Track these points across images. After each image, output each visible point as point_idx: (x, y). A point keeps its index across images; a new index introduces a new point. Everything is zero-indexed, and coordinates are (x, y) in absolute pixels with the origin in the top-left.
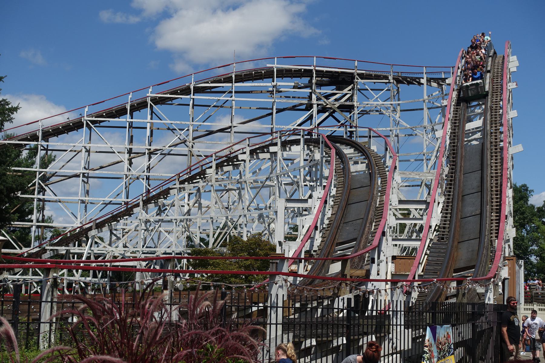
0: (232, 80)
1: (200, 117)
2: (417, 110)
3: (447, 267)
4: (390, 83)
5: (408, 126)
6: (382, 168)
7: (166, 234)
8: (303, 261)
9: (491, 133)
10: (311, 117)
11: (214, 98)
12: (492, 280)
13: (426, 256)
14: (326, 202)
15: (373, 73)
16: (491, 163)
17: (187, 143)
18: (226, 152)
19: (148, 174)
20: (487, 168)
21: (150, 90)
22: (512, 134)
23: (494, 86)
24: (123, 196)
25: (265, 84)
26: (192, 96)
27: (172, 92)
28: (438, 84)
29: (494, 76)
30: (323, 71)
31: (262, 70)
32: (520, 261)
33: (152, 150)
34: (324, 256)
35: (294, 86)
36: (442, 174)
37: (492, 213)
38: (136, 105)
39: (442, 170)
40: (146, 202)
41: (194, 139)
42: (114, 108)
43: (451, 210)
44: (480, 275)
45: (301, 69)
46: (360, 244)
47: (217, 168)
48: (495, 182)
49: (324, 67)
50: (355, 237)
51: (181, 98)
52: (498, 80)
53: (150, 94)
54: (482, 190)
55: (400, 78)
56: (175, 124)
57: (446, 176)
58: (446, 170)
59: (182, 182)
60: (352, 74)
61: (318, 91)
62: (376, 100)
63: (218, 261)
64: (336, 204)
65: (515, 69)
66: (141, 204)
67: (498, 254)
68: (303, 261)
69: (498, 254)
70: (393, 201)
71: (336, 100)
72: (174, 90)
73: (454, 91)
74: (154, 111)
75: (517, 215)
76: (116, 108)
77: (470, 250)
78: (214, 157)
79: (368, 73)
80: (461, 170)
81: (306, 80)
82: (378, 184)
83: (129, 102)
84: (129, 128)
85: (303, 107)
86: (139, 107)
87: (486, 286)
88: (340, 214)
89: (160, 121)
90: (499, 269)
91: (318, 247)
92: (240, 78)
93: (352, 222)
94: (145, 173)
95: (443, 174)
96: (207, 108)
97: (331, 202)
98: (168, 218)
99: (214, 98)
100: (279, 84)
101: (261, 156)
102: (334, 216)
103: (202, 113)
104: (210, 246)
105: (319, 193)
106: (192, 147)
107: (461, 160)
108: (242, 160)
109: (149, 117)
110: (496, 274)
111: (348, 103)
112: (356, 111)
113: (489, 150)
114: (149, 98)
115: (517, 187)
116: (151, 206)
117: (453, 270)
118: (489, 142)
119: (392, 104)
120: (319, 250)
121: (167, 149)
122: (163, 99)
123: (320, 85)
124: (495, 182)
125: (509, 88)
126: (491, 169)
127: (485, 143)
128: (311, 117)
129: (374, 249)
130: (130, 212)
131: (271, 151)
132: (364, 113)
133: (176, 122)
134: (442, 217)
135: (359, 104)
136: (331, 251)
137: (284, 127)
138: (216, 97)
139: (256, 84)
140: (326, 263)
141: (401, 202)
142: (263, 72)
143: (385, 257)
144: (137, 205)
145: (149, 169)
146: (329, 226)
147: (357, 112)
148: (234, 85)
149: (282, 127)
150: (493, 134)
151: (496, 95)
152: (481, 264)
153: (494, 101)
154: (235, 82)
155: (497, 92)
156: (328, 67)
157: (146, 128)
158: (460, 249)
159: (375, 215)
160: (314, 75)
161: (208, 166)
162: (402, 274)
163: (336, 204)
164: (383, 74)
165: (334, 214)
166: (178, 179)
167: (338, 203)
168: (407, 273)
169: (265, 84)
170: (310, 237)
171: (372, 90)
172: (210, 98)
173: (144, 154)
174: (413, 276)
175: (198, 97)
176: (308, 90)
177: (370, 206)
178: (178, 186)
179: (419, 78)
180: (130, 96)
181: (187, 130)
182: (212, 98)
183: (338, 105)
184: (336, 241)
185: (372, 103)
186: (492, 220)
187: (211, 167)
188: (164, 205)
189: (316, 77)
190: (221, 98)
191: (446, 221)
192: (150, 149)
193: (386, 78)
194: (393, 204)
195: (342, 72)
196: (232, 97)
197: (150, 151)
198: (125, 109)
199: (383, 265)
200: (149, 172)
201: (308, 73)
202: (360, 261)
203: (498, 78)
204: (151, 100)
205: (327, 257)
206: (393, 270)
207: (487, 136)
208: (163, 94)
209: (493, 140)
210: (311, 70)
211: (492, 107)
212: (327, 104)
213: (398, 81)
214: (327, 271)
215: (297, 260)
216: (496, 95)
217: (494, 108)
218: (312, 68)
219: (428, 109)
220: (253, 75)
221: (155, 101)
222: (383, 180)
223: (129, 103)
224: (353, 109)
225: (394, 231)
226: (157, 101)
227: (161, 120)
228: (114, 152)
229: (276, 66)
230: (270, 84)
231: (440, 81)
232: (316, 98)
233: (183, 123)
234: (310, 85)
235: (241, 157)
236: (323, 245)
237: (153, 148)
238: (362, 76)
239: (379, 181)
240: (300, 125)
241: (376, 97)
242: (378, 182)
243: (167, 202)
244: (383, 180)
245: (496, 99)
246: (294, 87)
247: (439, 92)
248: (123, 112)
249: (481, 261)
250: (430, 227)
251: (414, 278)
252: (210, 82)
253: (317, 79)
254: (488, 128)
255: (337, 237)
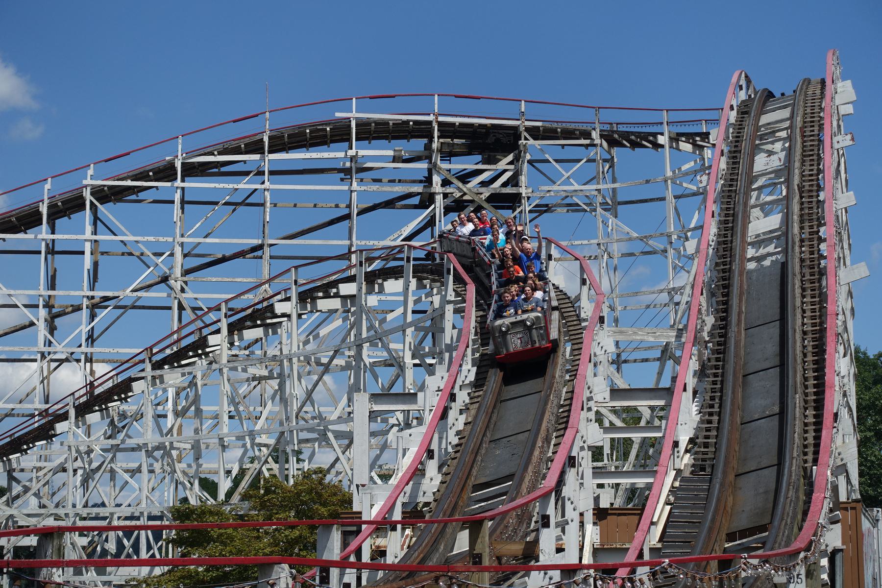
0: (263, 148)
1: (197, 226)
2: (652, 200)
3: (710, 529)
4: (595, 145)
5: (635, 235)
6: (575, 323)
7: (127, 476)
8: (399, 526)
9: (802, 241)
10: (431, 222)
11: (226, 186)
12: (802, 555)
13: (668, 508)
14: (453, 397)
15: (559, 127)
16: (803, 303)
17: (172, 282)
18: (250, 298)
19: (89, 350)
20: (795, 315)
21: (90, 172)
22: (850, 245)
23: (805, 142)
24: (37, 400)
25: (332, 155)
26: (178, 183)
27: (136, 175)
28: (694, 144)
29: (805, 122)
30: (453, 124)
31: (326, 124)
32: (875, 509)
33: (97, 300)
34: (444, 515)
35: (394, 157)
36: (702, 330)
37: (806, 409)
38: (60, 204)
39: (700, 321)
40: (83, 410)
41: (186, 272)
42: (14, 213)
43: (720, 407)
44: (780, 544)
45: (408, 122)
46: (521, 485)
47: (231, 332)
48: (811, 343)
49: (456, 116)
50: (512, 471)
51: (157, 187)
52: (813, 131)
53: (90, 179)
54: (783, 365)
55: (616, 136)
56: (143, 243)
57: (711, 334)
58: (710, 320)
59: (158, 366)
60: (515, 128)
61: (445, 166)
62: (567, 182)
63: (230, 531)
64: (476, 400)
65: (849, 109)
66: (72, 413)
67: (818, 497)
68: (399, 526)
69: (818, 497)
70: (596, 390)
71: (483, 184)
72: (142, 170)
73: (722, 155)
74: (99, 215)
75: (870, 415)
76: (17, 211)
77: (761, 490)
78: (224, 310)
79: (548, 125)
80: (739, 321)
81: (418, 144)
82: (564, 355)
83: (46, 197)
84: (47, 253)
85: (416, 200)
86: (68, 209)
87: (788, 570)
88: (481, 424)
89: (113, 238)
90: (818, 530)
91: (434, 493)
92: (279, 144)
93: (508, 439)
94: (84, 349)
95: (703, 330)
96: (212, 206)
97: (463, 397)
98: (131, 442)
99: (226, 186)
100: (361, 153)
101: (324, 304)
102: (469, 427)
103: (201, 217)
104: (222, 496)
105: (437, 381)
106: (183, 290)
107: (740, 300)
108: (284, 315)
109: (89, 228)
110: (811, 542)
111: (509, 190)
112: (527, 206)
113: (799, 277)
114: (89, 189)
115: (868, 357)
116: (94, 418)
117: (724, 536)
118: (797, 260)
119: (599, 190)
120: (435, 500)
121: (127, 294)
122: (117, 189)
123: (448, 154)
124: (811, 343)
125: (836, 146)
126: (803, 317)
127: (790, 263)
128: (431, 222)
129: (546, 496)
130: (49, 430)
131: (342, 294)
132: (542, 209)
133: (146, 238)
134: (702, 421)
135: (530, 190)
136: (460, 503)
137: (376, 243)
138: (228, 183)
139: (314, 155)
140: (449, 530)
141: (616, 393)
142: (328, 129)
143: (577, 513)
144: (64, 417)
145: (91, 338)
146: (459, 448)
147: (528, 209)
148: (267, 159)
149: (371, 243)
150: (807, 243)
151: (811, 160)
152: (782, 519)
153: (807, 173)
154: (270, 152)
155: (812, 155)
156: (464, 116)
157: (83, 253)
158: (740, 489)
159: (556, 422)
160: (436, 134)
161: (214, 328)
162: (616, 549)
163: (476, 400)
164: (581, 128)
165: (470, 423)
166: (150, 359)
167: (479, 399)
168: (627, 546)
169: (332, 155)
170: (417, 472)
171: (557, 161)
172: (217, 185)
173: (78, 308)
174: (637, 552)
175: (194, 184)
176: (423, 165)
177: (546, 403)
178: (149, 371)
179: (655, 135)
180: (48, 186)
181: (169, 256)
182: (221, 186)
183: (487, 195)
184: (472, 481)
185: (554, 191)
186: (806, 425)
187: (218, 331)
188: (123, 416)
189: (439, 137)
190: (241, 186)
191: (710, 431)
192: (93, 298)
193: (587, 135)
194: (598, 397)
195: (493, 125)
196: (263, 183)
197: (93, 301)
198: (39, 214)
199: (573, 528)
200: (92, 346)
201: (422, 130)
202: (520, 523)
203: (813, 126)
204: (92, 194)
205: (451, 515)
206: (597, 540)
207: (793, 247)
208: (118, 180)
209: (806, 256)
210: (430, 123)
211: (804, 187)
212: (465, 194)
213: (612, 139)
214: (450, 547)
215: (383, 525)
216: (811, 160)
217: (807, 188)
218: (431, 118)
219: (676, 197)
220: (308, 136)
221: (100, 195)
222: (576, 347)
223: (46, 202)
224: (520, 202)
225: (597, 453)
226: (104, 195)
227: (115, 235)
228: (16, 306)
229: (354, 114)
230: (341, 155)
231: (699, 139)
232: (440, 182)
233: (161, 239)
234: (427, 153)
235: (280, 308)
236: (442, 490)
237: (98, 294)
238: (535, 133)
239: (568, 349)
240: (409, 238)
241: (566, 175)
242: (565, 352)
243: (129, 407)
244: (576, 347)
245: (810, 170)
246: (395, 159)
247: (695, 161)
248: (33, 219)
249: (783, 514)
250: (676, 444)
251: (641, 555)
252: (216, 153)
253: (441, 140)
254: (796, 229)
255: (474, 472)
